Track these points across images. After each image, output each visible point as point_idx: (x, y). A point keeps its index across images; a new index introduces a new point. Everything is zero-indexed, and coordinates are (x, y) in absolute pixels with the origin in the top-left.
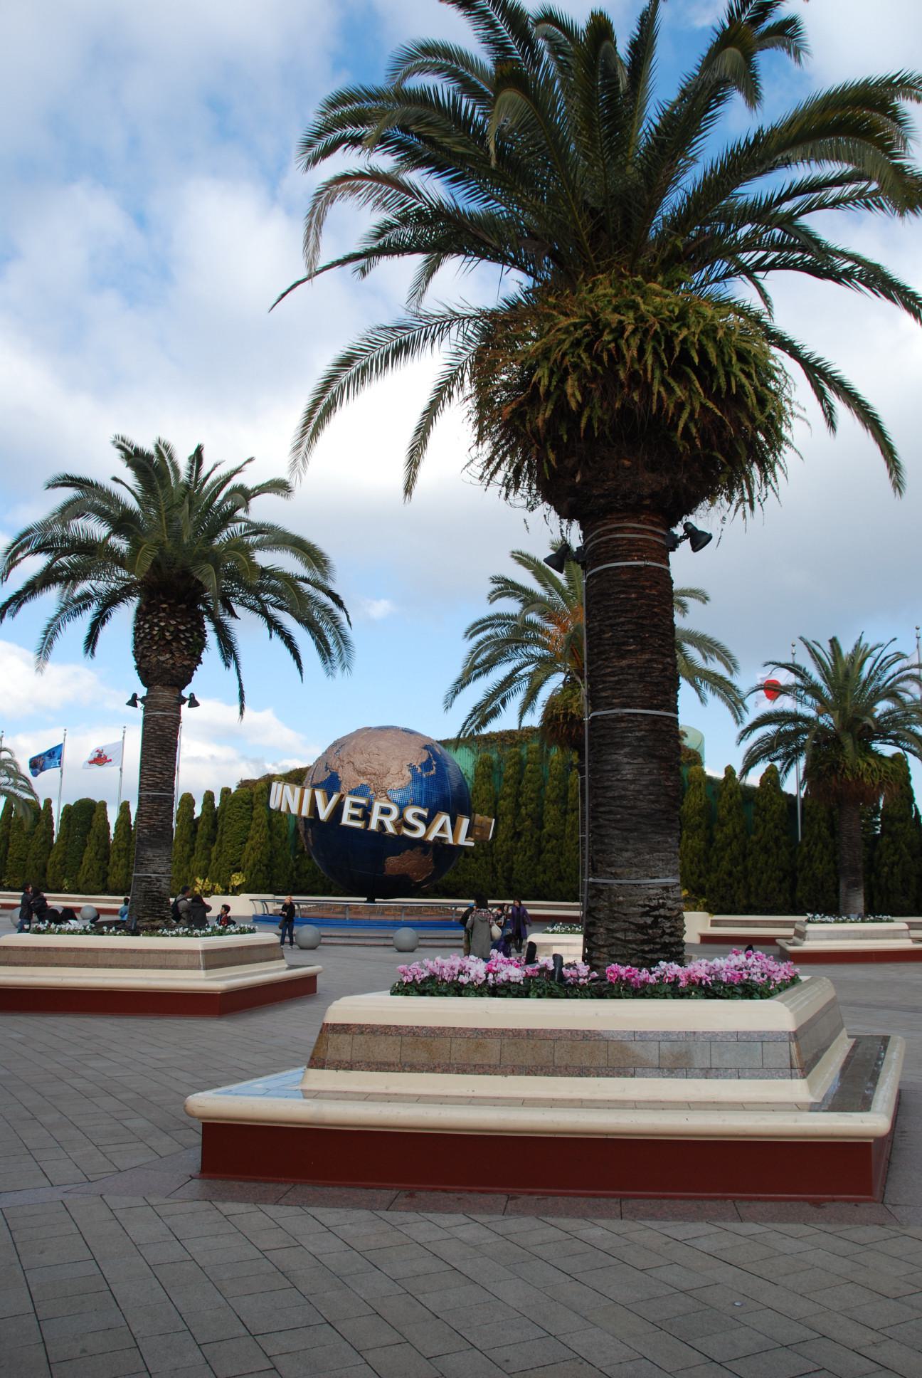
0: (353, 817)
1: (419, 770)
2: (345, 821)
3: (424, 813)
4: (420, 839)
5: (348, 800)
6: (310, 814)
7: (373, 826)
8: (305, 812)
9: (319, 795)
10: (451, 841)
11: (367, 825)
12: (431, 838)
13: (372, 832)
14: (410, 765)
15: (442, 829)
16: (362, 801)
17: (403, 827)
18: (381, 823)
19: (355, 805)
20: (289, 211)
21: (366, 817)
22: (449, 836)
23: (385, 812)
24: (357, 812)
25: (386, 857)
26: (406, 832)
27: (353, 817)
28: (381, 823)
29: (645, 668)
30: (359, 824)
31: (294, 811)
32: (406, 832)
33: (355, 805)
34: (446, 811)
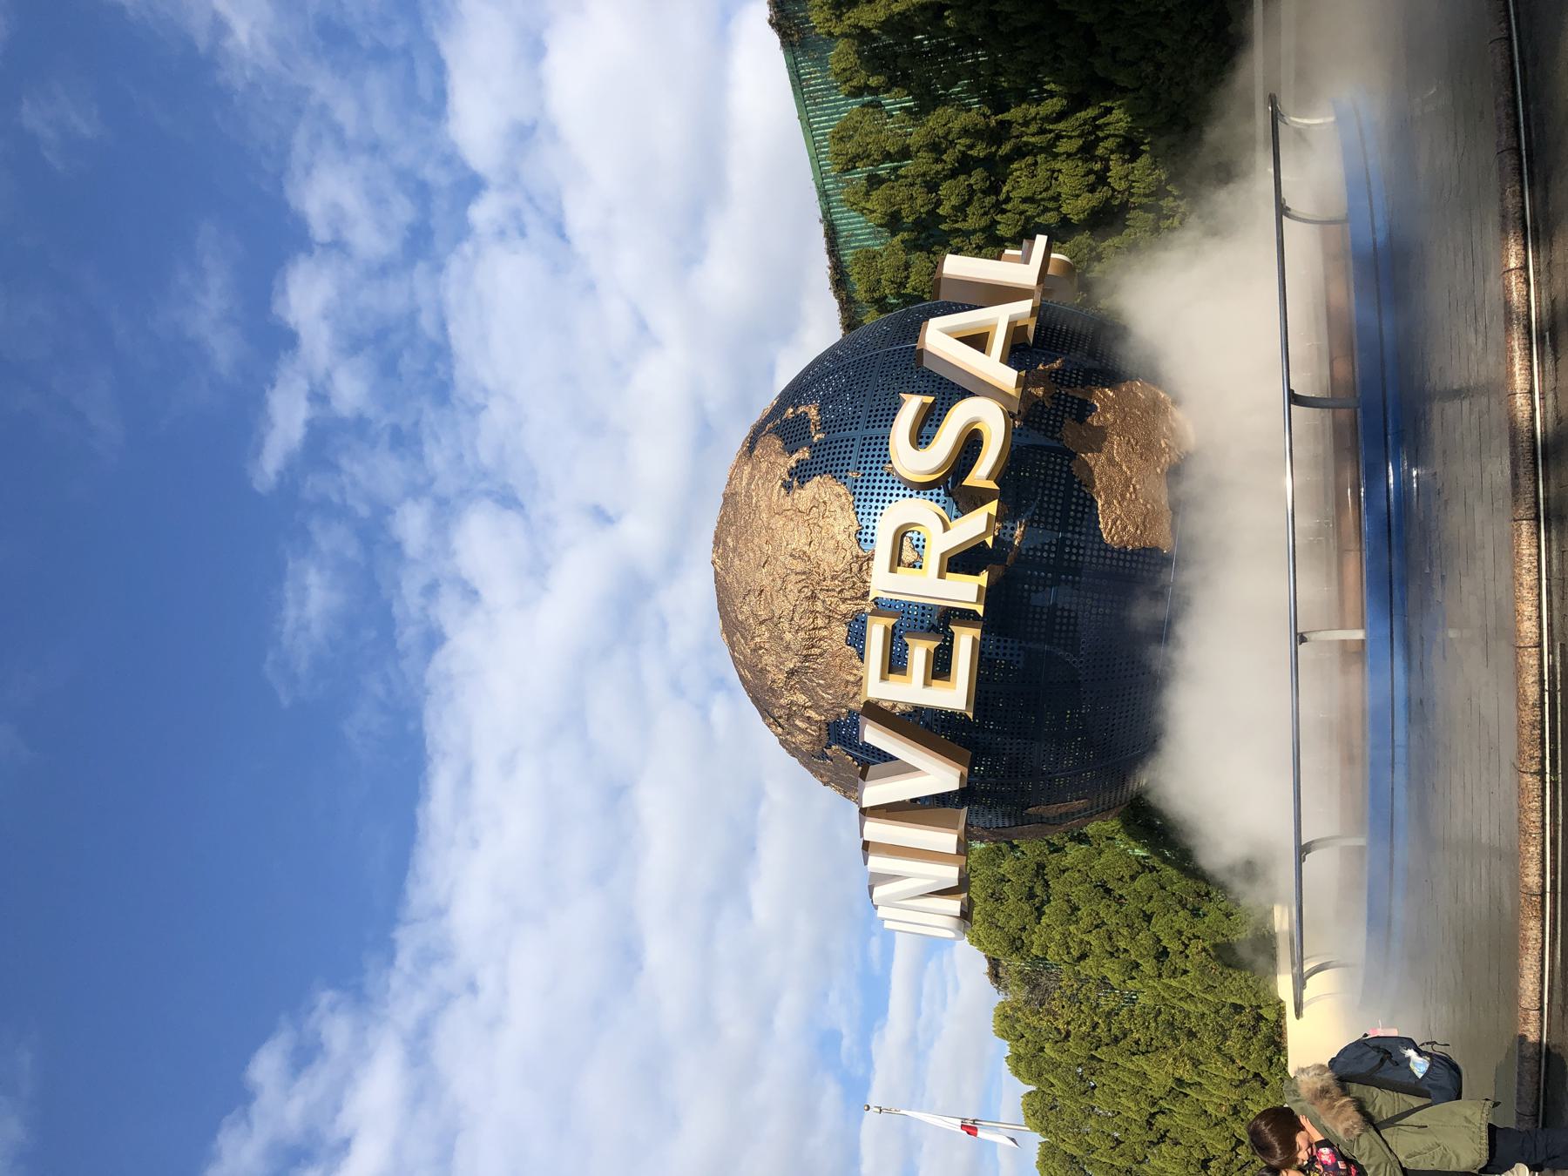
0: (940, 667)
1: (804, 454)
2: (954, 696)
3: (912, 405)
4: (1009, 416)
5: (880, 689)
6: (948, 825)
7: (966, 590)
8: (947, 840)
9: (877, 792)
10: (1024, 307)
11: (966, 617)
12: (1007, 378)
13: (990, 595)
14: (787, 487)
15: (978, 341)
16: (876, 632)
17: (969, 481)
18: (961, 561)
19: (895, 663)
20: (1231, 870)
21: (941, 622)
22: (999, 318)
23: (904, 543)
24: (919, 652)
25: (1108, 548)
26: (981, 474)
27: (940, 667)
28: (961, 561)
29: (1071, 344)
30: (965, 641)
31: (949, 874)
32: (981, 474)
33: (895, 663)
34: (914, 330)
